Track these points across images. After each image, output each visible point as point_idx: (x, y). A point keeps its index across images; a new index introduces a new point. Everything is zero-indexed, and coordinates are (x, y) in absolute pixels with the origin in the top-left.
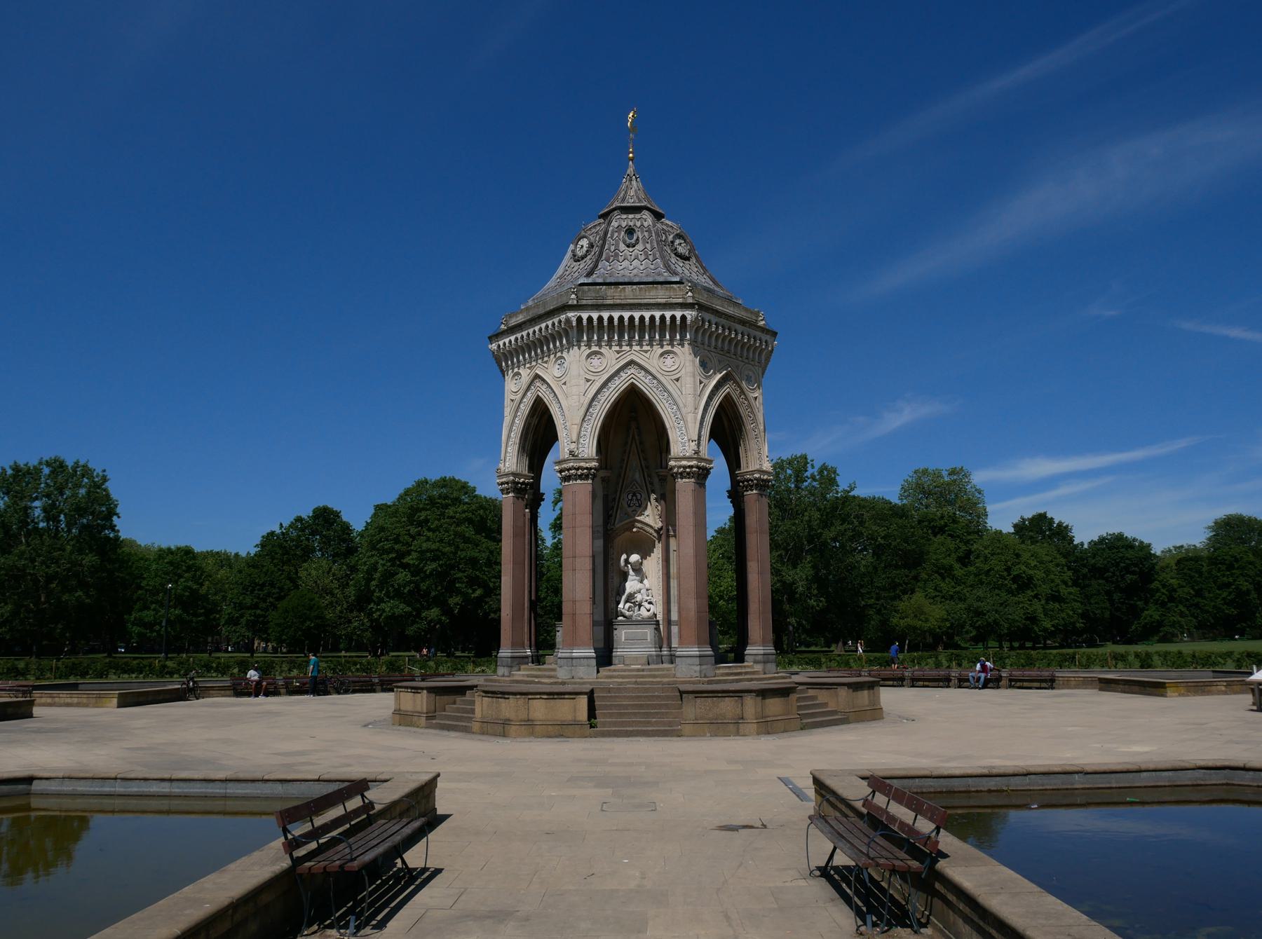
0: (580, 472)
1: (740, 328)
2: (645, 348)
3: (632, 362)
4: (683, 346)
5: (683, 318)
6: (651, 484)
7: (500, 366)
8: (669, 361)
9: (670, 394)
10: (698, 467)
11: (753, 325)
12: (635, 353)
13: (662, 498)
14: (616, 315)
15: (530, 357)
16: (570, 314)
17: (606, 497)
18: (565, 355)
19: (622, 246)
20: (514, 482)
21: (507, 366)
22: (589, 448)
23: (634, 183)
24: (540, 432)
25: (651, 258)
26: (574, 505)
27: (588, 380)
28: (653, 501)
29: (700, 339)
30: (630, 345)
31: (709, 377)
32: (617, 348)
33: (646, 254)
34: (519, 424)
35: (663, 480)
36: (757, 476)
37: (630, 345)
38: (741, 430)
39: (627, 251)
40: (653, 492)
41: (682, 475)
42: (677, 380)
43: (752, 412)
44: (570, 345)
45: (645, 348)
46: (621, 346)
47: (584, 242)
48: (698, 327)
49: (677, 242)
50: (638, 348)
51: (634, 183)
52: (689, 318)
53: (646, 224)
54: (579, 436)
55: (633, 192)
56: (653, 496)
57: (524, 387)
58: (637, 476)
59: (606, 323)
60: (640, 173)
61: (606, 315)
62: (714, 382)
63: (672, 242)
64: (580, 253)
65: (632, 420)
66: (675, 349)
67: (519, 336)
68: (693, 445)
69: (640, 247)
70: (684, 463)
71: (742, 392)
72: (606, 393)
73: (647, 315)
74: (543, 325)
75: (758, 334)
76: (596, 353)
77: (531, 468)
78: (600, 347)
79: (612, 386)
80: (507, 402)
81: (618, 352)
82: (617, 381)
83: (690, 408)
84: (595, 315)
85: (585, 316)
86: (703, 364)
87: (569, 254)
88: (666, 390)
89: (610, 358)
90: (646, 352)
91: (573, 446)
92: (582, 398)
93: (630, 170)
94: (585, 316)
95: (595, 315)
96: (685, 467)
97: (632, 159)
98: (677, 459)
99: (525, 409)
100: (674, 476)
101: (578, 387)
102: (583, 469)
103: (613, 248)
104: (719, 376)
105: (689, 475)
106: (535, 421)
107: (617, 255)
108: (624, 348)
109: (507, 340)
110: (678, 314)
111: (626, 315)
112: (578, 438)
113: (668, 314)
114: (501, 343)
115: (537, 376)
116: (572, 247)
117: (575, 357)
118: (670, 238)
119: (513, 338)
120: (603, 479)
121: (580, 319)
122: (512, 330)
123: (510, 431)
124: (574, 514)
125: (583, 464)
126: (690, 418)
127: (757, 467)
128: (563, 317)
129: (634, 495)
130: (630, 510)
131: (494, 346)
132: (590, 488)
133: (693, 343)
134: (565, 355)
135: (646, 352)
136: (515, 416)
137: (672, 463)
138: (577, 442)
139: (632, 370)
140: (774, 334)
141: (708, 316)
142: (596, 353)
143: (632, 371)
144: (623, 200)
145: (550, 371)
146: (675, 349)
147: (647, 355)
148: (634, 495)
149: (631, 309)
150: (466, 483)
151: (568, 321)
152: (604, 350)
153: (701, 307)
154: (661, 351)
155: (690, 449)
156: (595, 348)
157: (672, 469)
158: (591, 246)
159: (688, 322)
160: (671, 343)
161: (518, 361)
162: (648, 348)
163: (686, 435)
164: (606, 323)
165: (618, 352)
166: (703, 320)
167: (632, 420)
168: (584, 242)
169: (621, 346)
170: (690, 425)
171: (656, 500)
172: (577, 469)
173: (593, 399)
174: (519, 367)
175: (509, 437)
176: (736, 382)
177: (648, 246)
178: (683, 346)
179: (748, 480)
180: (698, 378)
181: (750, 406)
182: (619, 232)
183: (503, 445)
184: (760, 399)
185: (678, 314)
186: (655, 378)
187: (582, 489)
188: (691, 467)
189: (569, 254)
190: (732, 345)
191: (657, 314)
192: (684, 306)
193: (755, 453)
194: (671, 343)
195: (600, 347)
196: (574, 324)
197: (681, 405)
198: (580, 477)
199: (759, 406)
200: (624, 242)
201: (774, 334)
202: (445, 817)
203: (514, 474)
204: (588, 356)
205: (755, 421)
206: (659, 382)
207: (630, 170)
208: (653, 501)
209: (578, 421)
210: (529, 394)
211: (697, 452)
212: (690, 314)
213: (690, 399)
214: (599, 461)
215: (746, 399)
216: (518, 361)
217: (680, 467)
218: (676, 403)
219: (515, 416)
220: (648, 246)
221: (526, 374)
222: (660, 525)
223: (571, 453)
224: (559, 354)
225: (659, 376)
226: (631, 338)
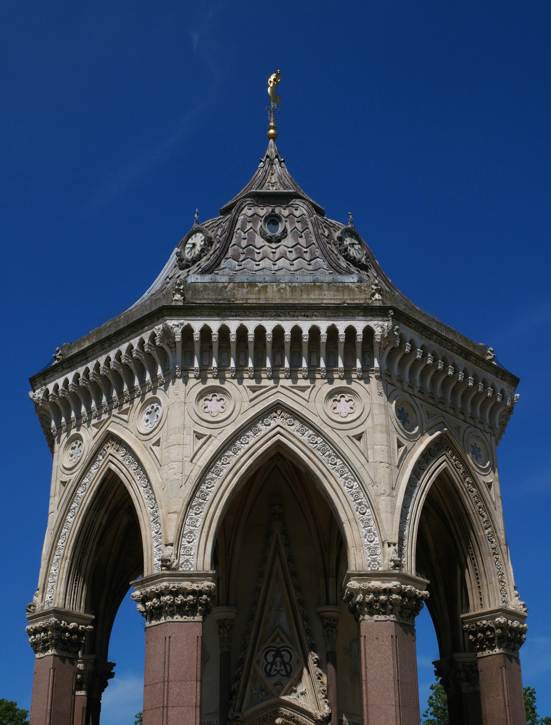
0: (179, 599)
1: (460, 361)
2: (301, 383)
3: (277, 407)
4: (367, 381)
5: (369, 332)
6: (309, 633)
7: (46, 425)
8: (343, 406)
9: (346, 462)
10: (400, 592)
11: (480, 361)
12: (283, 391)
13: (328, 660)
14: (251, 325)
15: (99, 405)
16: (171, 323)
17: (225, 657)
18: (160, 394)
19: (259, 241)
20: (56, 628)
21: (59, 426)
22: (199, 557)
23: (277, 167)
24: (111, 535)
25: (307, 256)
26: (167, 664)
27: (199, 436)
28: (313, 666)
29: (395, 371)
30: (275, 378)
31: (413, 438)
32: (253, 383)
33: (299, 251)
34: (74, 522)
35: (330, 626)
36: (501, 620)
37: (275, 378)
38: (467, 539)
39: (267, 248)
40: (313, 648)
41: (372, 608)
42: (359, 437)
43: (486, 508)
44: (170, 376)
45: (301, 383)
46: (258, 379)
47: (198, 239)
48: (394, 350)
49: (348, 241)
50: (288, 383)
51: (277, 167)
52: (378, 331)
53: (297, 213)
54: (180, 535)
55: (275, 176)
56: (313, 657)
57: (86, 457)
58: (283, 620)
59: (233, 338)
60: (284, 156)
61: (233, 325)
62: (421, 448)
63: (341, 239)
64: (188, 255)
65: (278, 511)
66: (354, 386)
67: (81, 370)
68: (391, 552)
69: (289, 241)
70: (376, 584)
71: (468, 472)
72: (231, 458)
73: (305, 326)
74: (124, 348)
75: (490, 376)
76: (214, 390)
77: (92, 604)
78: (223, 380)
79: (242, 446)
80: (55, 487)
81: (253, 389)
82: (251, 438)
83: (384, 487)
84: (215, 325)
85: (197, 325)
86: (402, 415)
87: (173, 259)
88: (339, 454)
89: (240, 400)
90: (303, 389)
91: (169, 552)
92: (188, 466)
93: (272, 149)
94: (197, 325)
95: (215, 325)
96: (377, 592)
97: (274, 137)
98: (362, 576)
99: (85, 496)
100: (355, 612)
101: (177, 453)
102: (185, 593)
103: (244, 243)
104: (428, 439)
105: (384, 608)
106: (102, 518)
107: (251, 252)
108: (264, 382)
109: (60, 381)
110: (359, 326)
111: (269, 325)
112: (178, 537)
113: (342, 326)
114: (50, 387)
115: (110, 437)
116: (176, 250)
117: (178, 398)
118: (337, 234)
119: (70, 376)
120: (221, 624)
121: (188, 331)
122: (70, 363)
123: (57, 536)
124: (166, 681)
125: (186, 585)
126: (383, 504)
127: (499, 604)
128: (158, 329)
129: (278, 653)
130: (270, 682)
131: (38, 394)
132: (198, 630)
133: (385, 377)
134: (160, 394)
135: (303, 389)
136: (67, 510)
137: (353, 584)
138: (177, 543)
139: (277, 420)
140: (515, 381)
141: (409, 333)
142: (214, 390)
143: (279, 421)
144: (261, 185)
145: (132, 425)
146: (354, 386)
147: (305, 395)
148: (278, 653)
149: (277, 316)
150: (13, 704)
151: (167, 333)
152: (230, 385)
153: (399, 317)
154: (328, 388)
155: (385, 559)
156: (212, 382)
157: (353, 593)
158: (209, 242)
159: (378, 339)
160: (347, 375)
161: (79, 416)
162: (307, 383)
163: (376, 538)
164: (233, 338)
165: (253, 389)
166: (401, 336)
167: (278, 511)
168: (198, 239)
169: (258, 379)
170: (384, 516)
171: (319, 663)
172: (175, 593)
173: (208, 469)
174: (78, 427)
175: (54, 547)
176: (456, 453)
177: (302, 241)
178: (367, 381)
179: (483, 630)
180: (395, 436)
181: (481, 497)
182: (255, 222)
183: (44, 564)
184: (496, 489)
185: (359, 326)
186: (318, 432)
187: (184, 634)
188: (388, 592)
189: (173, 259)
190: (447, 394)
191: (323, 325)
192: (368, 311)
193: (495, 579)
194: (347, 375)
195: (223, 380)
196: (178, 338)
197: (367, 480)
198: (181, 609)
199: (494, 495)
200: (263, 235)
201: (515, 381)
202: (433, 663)
203: (56, 612)
204: (201, 395)
205: (490, 523)
206: (327, 440)
207: (272, 149)
208: (313, 666)
209: (179, 505)
210: (93, 470)
211: (398, 565)
212: (380, 326)
213: (382, 472)
214: (216, 579)
215: (475, 484)
216: (79, 416)
217: (367, 592)
218: (357, 477)
219: (67, 510)
220: (302, 241)
221: (89, 436)
222: (326, 710)
223: (165, 562)
224: (149, 395)
225: (327, 430)
226: (277, 366)
